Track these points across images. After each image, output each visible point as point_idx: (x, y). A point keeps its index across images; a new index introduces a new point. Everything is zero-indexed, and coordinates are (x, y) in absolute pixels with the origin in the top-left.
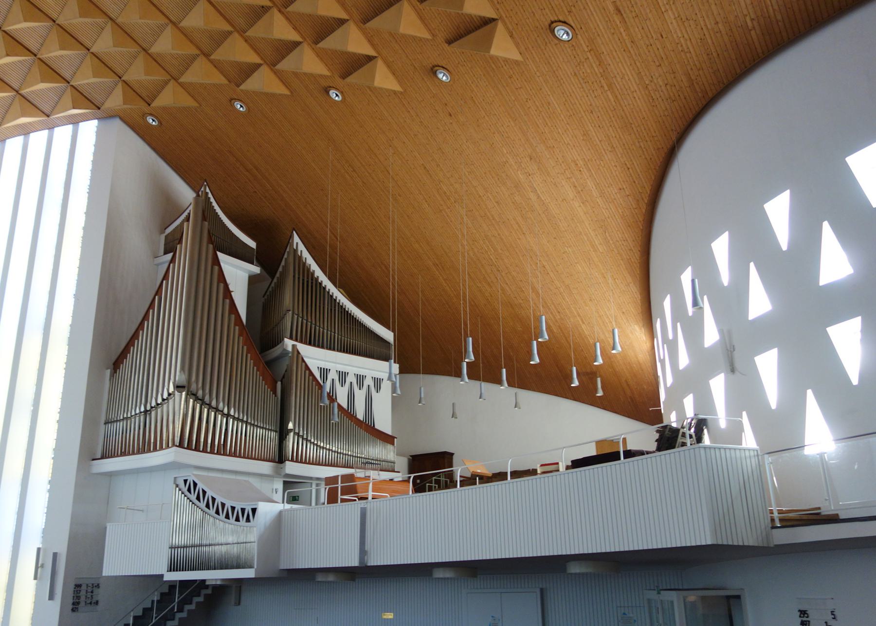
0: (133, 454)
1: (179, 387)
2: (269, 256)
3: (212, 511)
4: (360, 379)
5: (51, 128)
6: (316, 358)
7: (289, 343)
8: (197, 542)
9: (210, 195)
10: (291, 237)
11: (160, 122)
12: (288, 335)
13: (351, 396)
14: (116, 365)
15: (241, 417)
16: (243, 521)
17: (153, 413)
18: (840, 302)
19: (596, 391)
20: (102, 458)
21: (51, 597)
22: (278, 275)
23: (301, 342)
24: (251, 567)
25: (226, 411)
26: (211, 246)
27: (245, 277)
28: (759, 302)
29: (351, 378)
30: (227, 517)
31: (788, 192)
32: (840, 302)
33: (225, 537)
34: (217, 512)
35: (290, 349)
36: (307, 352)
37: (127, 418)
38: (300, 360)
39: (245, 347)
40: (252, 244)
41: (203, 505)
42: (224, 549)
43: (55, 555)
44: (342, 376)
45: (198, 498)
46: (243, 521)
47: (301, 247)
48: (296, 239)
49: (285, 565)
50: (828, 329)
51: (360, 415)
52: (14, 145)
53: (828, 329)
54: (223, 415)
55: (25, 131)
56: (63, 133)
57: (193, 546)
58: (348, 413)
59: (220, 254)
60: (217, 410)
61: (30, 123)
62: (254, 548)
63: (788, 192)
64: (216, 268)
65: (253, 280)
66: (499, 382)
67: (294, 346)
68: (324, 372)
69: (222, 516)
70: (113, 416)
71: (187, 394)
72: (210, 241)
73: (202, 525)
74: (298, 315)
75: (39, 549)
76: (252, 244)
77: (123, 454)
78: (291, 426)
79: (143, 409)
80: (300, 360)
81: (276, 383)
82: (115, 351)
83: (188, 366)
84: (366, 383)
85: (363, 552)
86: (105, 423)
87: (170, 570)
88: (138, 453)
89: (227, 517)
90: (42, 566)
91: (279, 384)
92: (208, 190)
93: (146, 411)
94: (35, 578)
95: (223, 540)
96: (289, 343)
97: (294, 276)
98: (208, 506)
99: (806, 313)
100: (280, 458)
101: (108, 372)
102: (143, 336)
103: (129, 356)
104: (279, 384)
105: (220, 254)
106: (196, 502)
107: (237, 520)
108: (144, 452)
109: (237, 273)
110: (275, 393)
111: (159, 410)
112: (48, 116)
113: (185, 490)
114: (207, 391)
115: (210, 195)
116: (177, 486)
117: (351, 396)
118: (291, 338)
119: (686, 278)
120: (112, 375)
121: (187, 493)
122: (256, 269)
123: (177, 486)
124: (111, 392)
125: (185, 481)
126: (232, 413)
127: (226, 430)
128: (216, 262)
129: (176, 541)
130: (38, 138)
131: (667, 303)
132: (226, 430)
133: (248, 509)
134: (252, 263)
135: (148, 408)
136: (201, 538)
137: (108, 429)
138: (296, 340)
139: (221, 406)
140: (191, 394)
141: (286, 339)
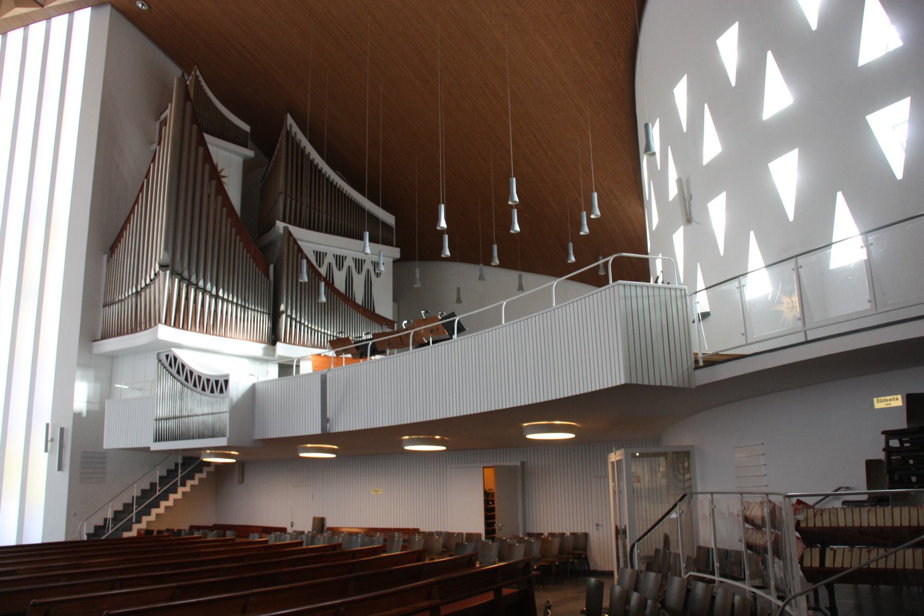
0: (128, 333)
1: (163, 267)
2: (264, 139)
3: (191, 384)
4: (359, 263)
5: (49, 18)
6: (310, 241)
7: (280, 225)
8: (178, 414)
9: (201, 79)
10: (283, 121)
11: (149, 6)
12: (281, 216)
13: (349, 281)
14: (112, 249)
15: (230, 299)
16: (217, 393)
17: (143, 294)
18: (883, 84)
19: (567, 256)
20: (103, 338)
21: (60, 468)
22: (274, 158)
23: (295, 224)
24: (224, 436)
25: (214, 292)
26: (195, 127)
27: (239, 161)
28: (778, 95)
29: (349, 262)
30: (203, 389)
31: (724, 193)
32: (883, 84)
33: (202, 408)
34: (195, 385)
35: (281, 231)
36: (298, 233)
37: (121, 300)
38: (292, 241)
39: (234, 229)
40: (246, 128)
41: (182, 378)
42: (210, 419)
43: (62, 430)
44: (340, 260)
45: (178, 372)
46: (217, 393)
47: (295, 129)
48: (290, 120)
49: (258, 435)
50: (868, 117)
51: (359, 299)
52: (15, 36)
53: (868, 117)
54: (211, 296)
55: (25, 22)
56: (60, 22)
57: (175, 418)
58: (347, 298)
59: (208, 138)
60: (204, 291)
61: (26, 14)
62: (226, 417)
63: (724, 193)
64: (201, 149)
65: (248, 167)
66: (488, 262)
67: (286, 229)
68: (320, 256)
69: (208, 392)
70: (109, 299)
71: (172, 274)
72: (195, 119)
73: (181, 398)
74: (291, 198)
75: (48, 425)
76: (246, 128)
77: (119, 334)
78: (282, 308)
79: (134, 291)
80: (292, 241)
81: (269, 266)
82: (108, 235)
83: (171, 244)
84: (365, 268)
85: (325, 420)
86: (104, 306)
87: (156, 440)
88: (132, 332)
89: (203, 389)
90: (52, 440)
91: (272, 267)
92: (198, 73)
93: (137, 292)
94: (46, 451)
95: (200, 412)
96: (280, 225)
97: (287, 158)
98: (186, 379)
99: (840, 93)
100: (274, 338)
101: (105, 257)
102: (134, 218)
103: (123, 240)
104: (272, 267)
105: (208, 138)
106: (177, 375)
107: (212, 391)
108: (136, 331)
109: (230, 159)
110: (267, 275)
111: (148, 290)
112: (42, 6)
113: (167, 364)
114: (186, 265)
115: (201, 79)
116: (160, 361)
117: (349, 281)
118: (284, 220)
119: (681, 92)
120: (108, 260)
121: (169, 368)
122: (250, 153)
123: (160, 361)
124: (107, 276)
125: (167, 356)
126: (221, 294)
127: (216, 311)
128: (203, 143)
129: (162, 412)
130: (37, 29)
131: (655, 132)
132: (216, 311)
133: (222, 381)
134: (246, 146)
135: (139, 289)
136: (181, 410)
137: (104, 312)
138: (290, 223)
139: (209, 287)
140: (174, 274)
141: (278, 222)
